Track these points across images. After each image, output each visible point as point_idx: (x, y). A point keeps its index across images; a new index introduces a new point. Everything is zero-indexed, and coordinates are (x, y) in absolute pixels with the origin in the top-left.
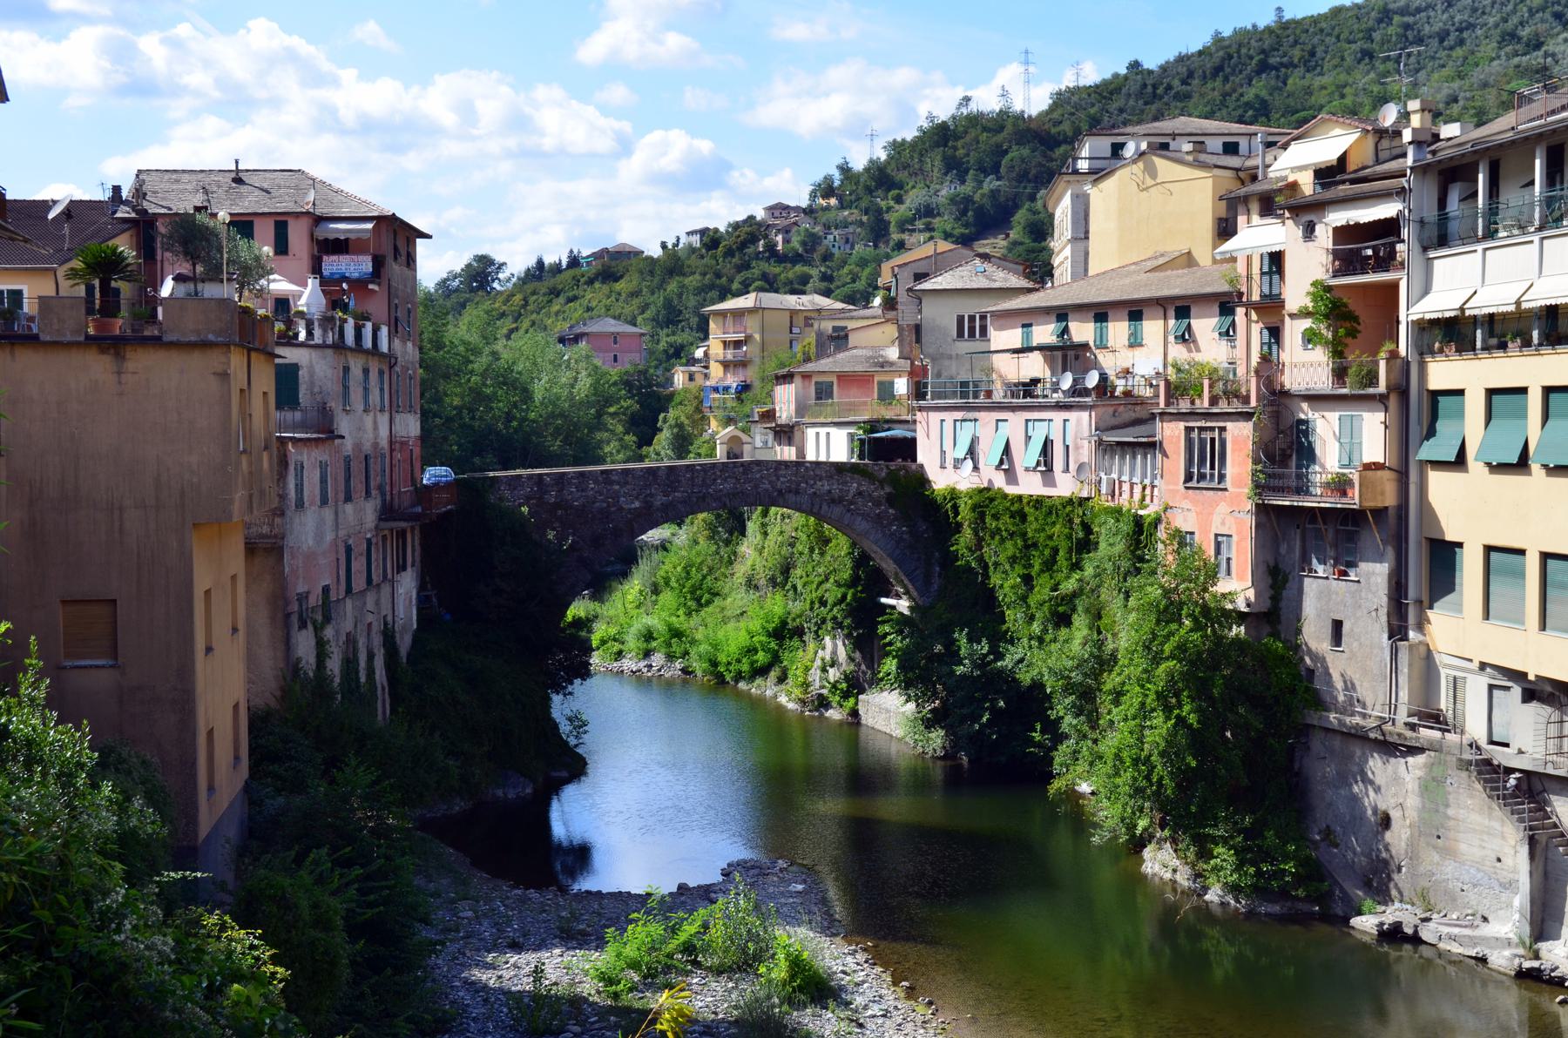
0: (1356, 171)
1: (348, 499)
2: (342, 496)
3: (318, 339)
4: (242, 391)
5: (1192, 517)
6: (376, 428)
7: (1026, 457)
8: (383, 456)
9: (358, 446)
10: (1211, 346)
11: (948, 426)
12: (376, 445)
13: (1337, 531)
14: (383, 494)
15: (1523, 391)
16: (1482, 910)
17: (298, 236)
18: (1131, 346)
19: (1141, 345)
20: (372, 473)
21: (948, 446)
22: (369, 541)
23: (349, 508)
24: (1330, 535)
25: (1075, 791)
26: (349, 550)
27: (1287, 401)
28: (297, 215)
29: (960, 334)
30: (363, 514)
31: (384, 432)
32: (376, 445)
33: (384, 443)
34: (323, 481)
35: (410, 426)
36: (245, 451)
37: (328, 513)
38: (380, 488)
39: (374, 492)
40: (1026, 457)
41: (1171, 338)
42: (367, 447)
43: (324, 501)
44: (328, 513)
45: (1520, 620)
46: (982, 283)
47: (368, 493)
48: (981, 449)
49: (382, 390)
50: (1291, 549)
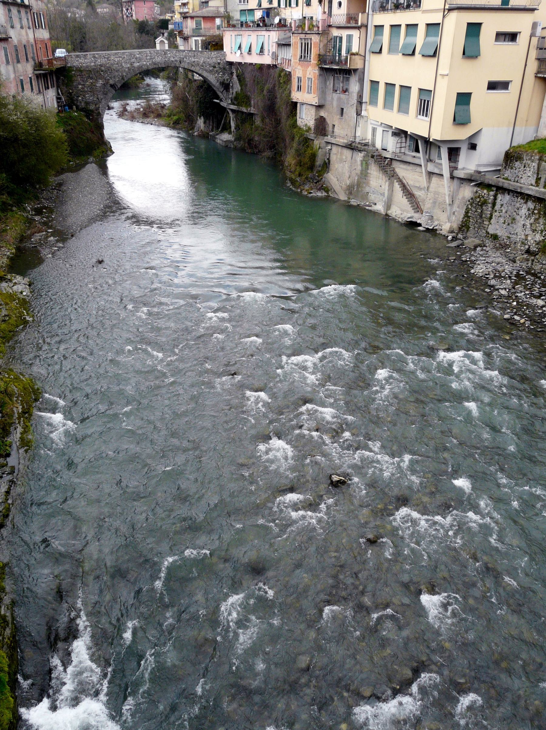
1: (18, 62)
2: (16, 61)
6: (27, 35)
8: (32, 45)
9: (20, 41)
11: (233, 37)
13: (343, 77)
14: (34, 60)
15: (400, 25)
16: (375, 202)
20: (28, 52)
22: (31, 78)
25: (38, 252)
26: (22, 81)
31: (31, 36)
32: (28, 41)
33: (32, 40)
41: (305, 5)
45: (392, 109)
48: (243, 47)
49: (28, 19)
50: (330, 84)
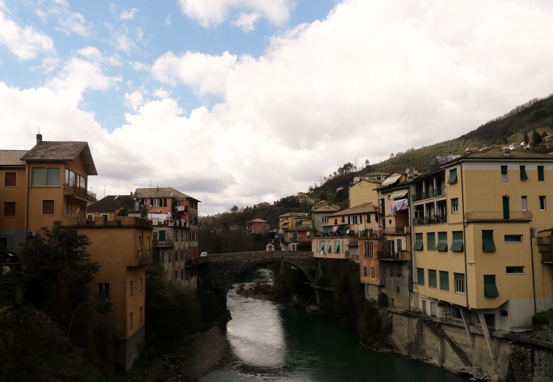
0: (356, 207)
3: (170, 225)
4: (140, 237)
5: (366, 263)
7: (326, 249)
9: (179, 249)
10: (374, 226)
11: (318, 243)
12: (184, 248)
17: (169, 202)
18: (544, 197)
19: (540, 197)
21: (318, 248)
22: (182, 270)
23: (177, 263)
24: (210, 221)
27: (385, 236)
28: (169, 198)
29: (323, 221)
30: (181, 264)
32: (184, 248)
34: (170, 257)
35: (195, 244)
36: (140, 251)
37: (171, 264)
38: (186, 258)
39: (184, 259)
40: (334, 250)
42: (182, 248)
43: (170, 261)
44: (171, 264)
46: (328, 210)
47: (182, 259)
